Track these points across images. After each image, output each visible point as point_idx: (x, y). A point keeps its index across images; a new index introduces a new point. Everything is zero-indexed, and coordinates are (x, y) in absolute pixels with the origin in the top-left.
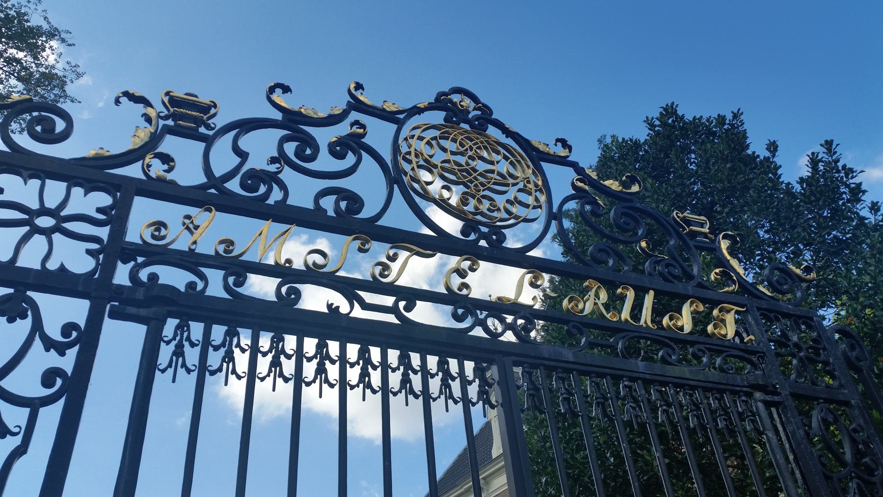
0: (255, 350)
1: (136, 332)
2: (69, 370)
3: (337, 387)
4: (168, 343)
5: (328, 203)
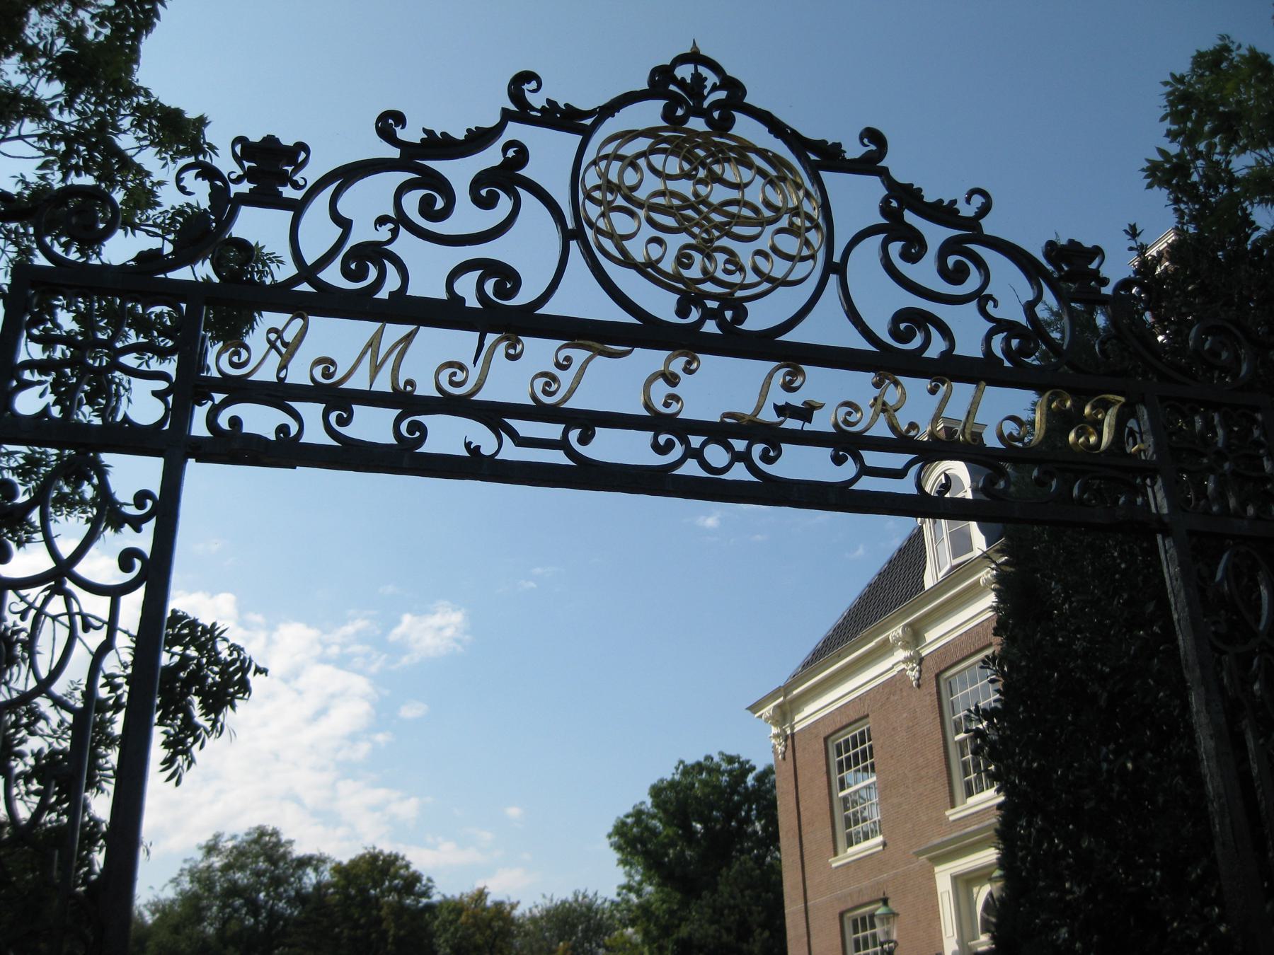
5: (466, 287)
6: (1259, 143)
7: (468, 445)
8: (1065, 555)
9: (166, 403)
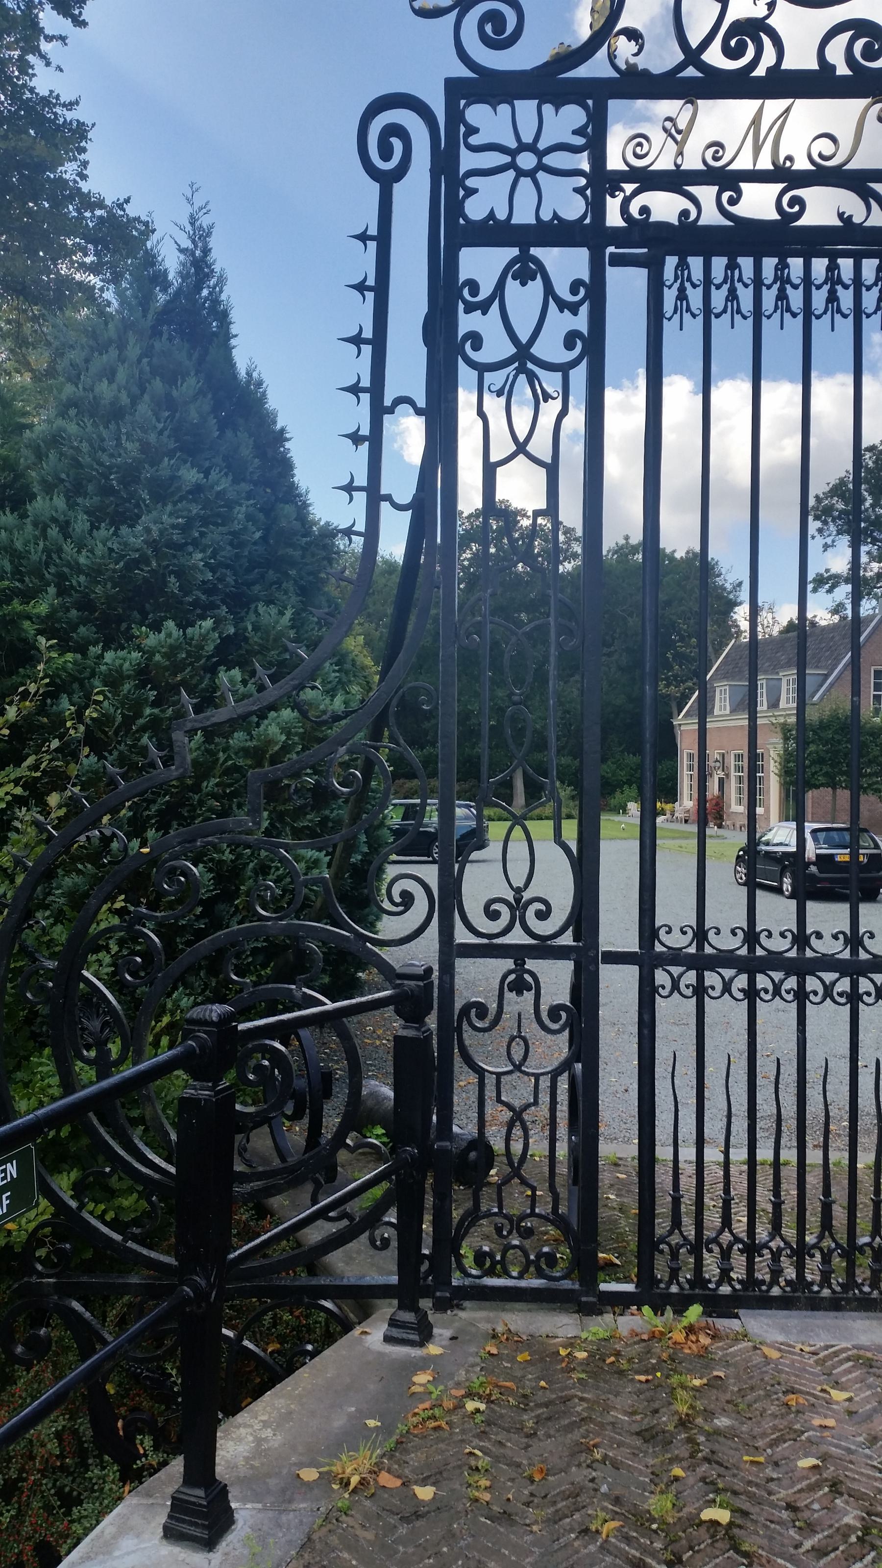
0: (758, 282)
1: (639, 277)
2: (584, 329)
3: (851, 317)
4: (670, 287)
5: (836, 53)
6: (879, 562)
7: (841, 215)
8: (347, 1502)
9: (585, 197)
